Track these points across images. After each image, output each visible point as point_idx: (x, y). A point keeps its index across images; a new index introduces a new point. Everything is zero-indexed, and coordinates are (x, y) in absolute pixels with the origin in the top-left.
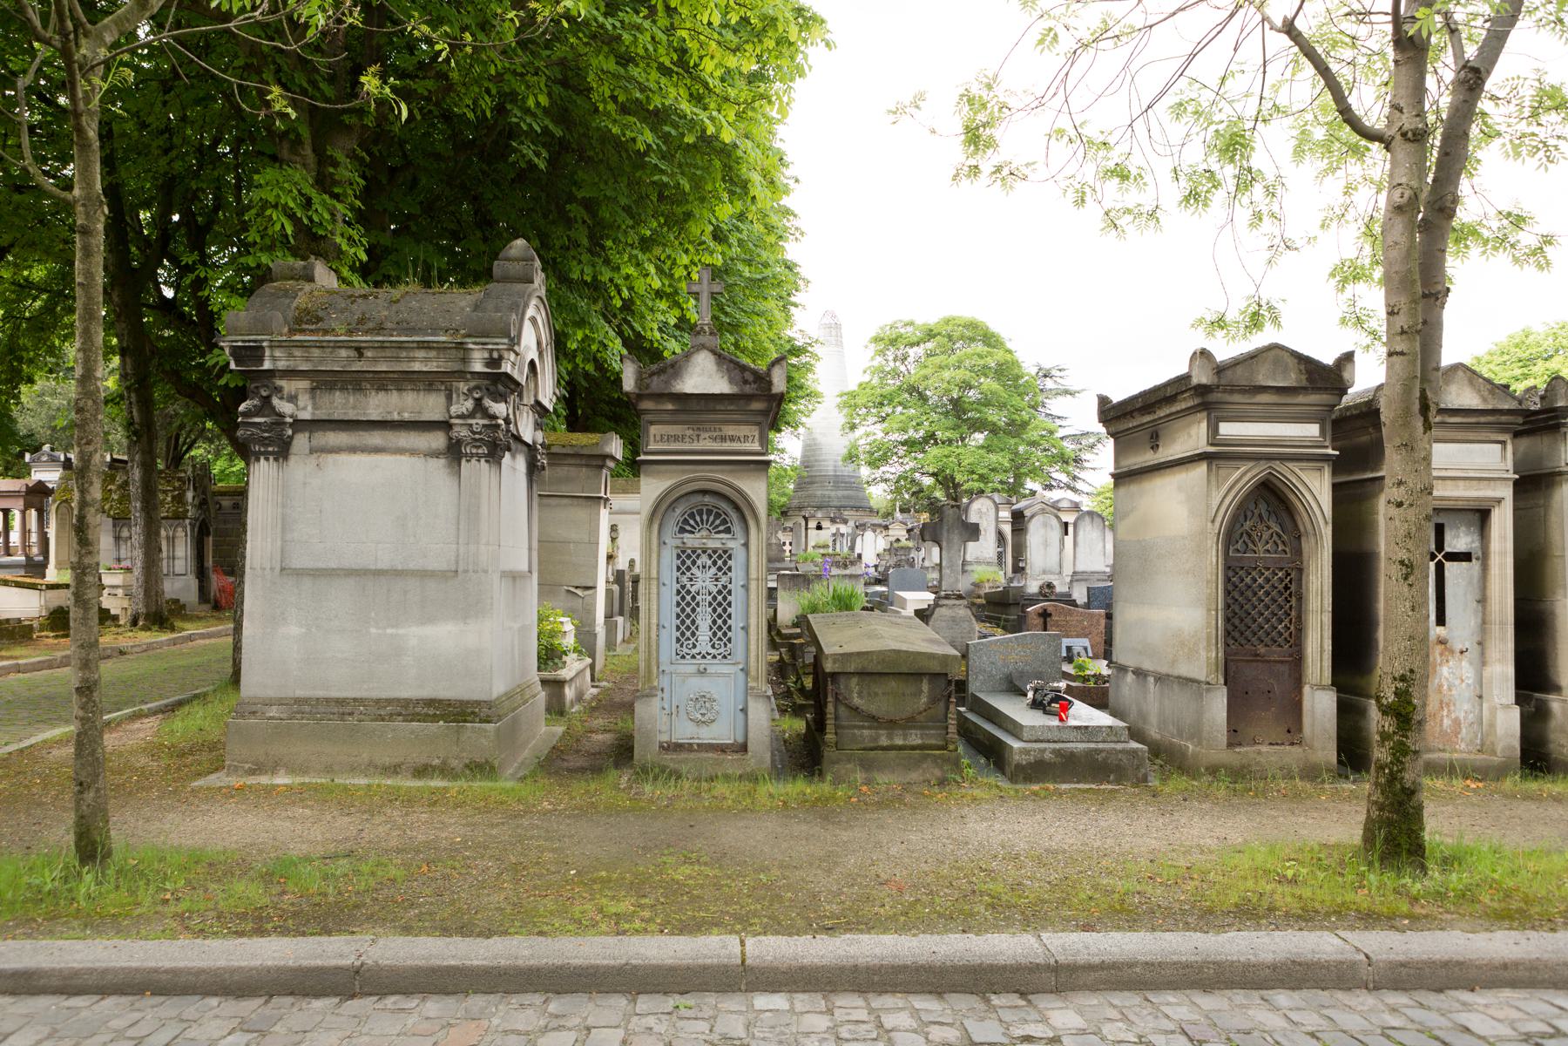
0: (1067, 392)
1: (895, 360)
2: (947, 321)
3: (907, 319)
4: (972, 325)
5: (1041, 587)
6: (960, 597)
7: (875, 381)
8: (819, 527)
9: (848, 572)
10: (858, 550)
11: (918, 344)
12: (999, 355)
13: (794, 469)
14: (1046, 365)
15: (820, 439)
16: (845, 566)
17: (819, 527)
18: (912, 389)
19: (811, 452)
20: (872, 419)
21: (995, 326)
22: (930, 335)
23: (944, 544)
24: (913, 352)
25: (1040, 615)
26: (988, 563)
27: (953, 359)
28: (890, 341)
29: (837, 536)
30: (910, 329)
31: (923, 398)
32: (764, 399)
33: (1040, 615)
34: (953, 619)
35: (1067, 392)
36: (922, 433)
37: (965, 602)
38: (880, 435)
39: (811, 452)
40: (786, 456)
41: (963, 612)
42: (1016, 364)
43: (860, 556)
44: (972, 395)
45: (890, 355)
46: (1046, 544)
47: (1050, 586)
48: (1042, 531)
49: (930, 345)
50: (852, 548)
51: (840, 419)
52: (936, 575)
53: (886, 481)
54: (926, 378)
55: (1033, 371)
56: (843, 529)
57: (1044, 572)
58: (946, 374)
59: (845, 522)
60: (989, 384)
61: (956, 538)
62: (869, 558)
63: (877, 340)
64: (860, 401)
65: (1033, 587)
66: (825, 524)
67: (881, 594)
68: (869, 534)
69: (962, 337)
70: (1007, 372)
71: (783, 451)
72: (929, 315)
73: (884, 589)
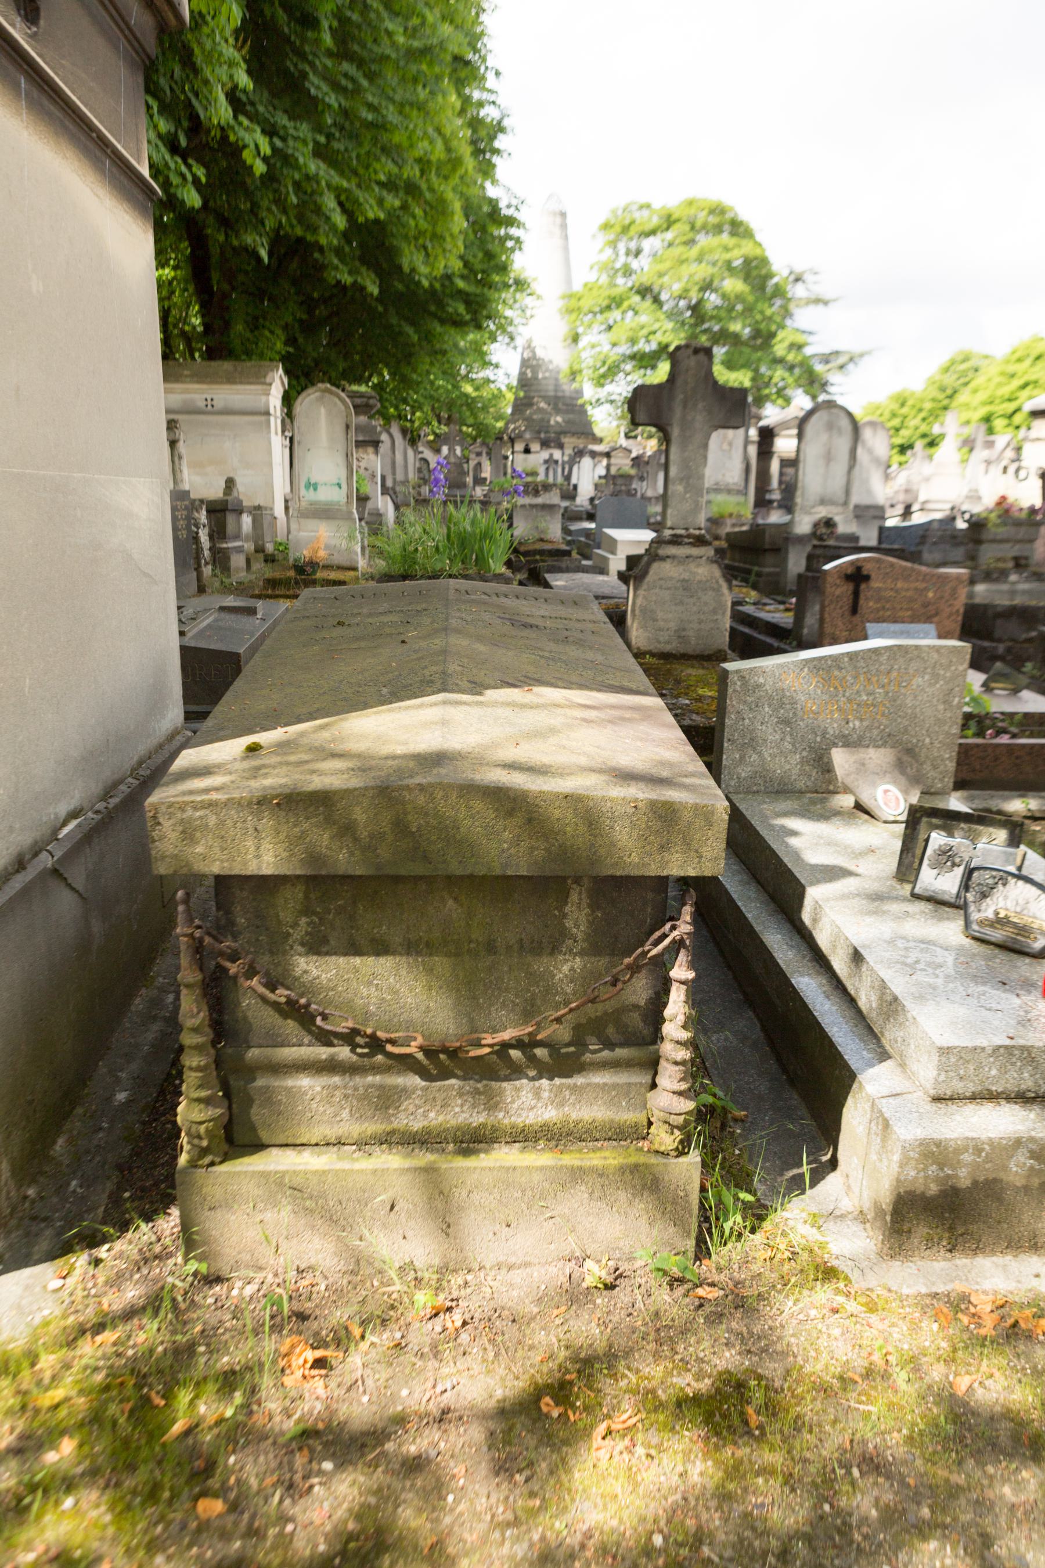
0: (818, 301)
1: (627, 254)
2: (690, 203)
3: (643, 200)
4: (718, 210)
5: (816, 525)
6: (700, 541)
7: (604, 279)
8: (527, 451)
9: (539, 500)
10: (574, 481)
11: (653, 232)
12: (747, 248)
13: (509, 388)
14: (798, 268)
15: (540, 353)
16: (536, 493)
17: (527, 451)
18: (644, 291)
19: (530, 364)
20: (597, 327)
21: (744, 214)
22: (669, 222)
23: (675, 432)
24: (649, 244)
25: (848, 578)
26: (729, 491)
27: (694, 252)
28: (624, 229)
29: (550, 462)
30: (646, 213)
31: (656, 300)
32: (475, 294)
33: (848, 578)
34: (686, 585)
35: (818, 301)
36: (654, 346)
37: (709, 552)
38: (606, 347)
39: (530, 364)
40: (500, 372)
41: (705, 570)
42: (764, 261)
43: (575, 487)
44: (713, 299)
45: (622, 247)
46: (829, 457)
47: (829, 523)
48: (824, 437)
49: (669, 236)
50: (568, 478)
51: (560, 328)
52: (658, 509)
53: (612, 402)
54: (661, 275)
55: (785, 273)
56: (557, 454)
57: (823, 502)
58: (686, 270)
59: (561, 446)
60: (733, 285)
61: (699, 419)
62: (586, 490)
63: (606, 226)
64: (586, 304)
65: (803, 525)
66: (535, 447)
67: (587, 533)
68: (586, 462)
69: (704, 227)
70: (755, 270)
71: (497, 366)
72: (667, 196)
73: (593, 526)
